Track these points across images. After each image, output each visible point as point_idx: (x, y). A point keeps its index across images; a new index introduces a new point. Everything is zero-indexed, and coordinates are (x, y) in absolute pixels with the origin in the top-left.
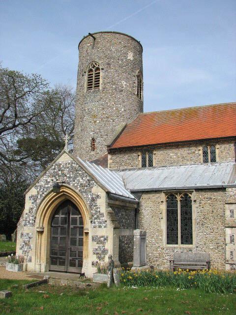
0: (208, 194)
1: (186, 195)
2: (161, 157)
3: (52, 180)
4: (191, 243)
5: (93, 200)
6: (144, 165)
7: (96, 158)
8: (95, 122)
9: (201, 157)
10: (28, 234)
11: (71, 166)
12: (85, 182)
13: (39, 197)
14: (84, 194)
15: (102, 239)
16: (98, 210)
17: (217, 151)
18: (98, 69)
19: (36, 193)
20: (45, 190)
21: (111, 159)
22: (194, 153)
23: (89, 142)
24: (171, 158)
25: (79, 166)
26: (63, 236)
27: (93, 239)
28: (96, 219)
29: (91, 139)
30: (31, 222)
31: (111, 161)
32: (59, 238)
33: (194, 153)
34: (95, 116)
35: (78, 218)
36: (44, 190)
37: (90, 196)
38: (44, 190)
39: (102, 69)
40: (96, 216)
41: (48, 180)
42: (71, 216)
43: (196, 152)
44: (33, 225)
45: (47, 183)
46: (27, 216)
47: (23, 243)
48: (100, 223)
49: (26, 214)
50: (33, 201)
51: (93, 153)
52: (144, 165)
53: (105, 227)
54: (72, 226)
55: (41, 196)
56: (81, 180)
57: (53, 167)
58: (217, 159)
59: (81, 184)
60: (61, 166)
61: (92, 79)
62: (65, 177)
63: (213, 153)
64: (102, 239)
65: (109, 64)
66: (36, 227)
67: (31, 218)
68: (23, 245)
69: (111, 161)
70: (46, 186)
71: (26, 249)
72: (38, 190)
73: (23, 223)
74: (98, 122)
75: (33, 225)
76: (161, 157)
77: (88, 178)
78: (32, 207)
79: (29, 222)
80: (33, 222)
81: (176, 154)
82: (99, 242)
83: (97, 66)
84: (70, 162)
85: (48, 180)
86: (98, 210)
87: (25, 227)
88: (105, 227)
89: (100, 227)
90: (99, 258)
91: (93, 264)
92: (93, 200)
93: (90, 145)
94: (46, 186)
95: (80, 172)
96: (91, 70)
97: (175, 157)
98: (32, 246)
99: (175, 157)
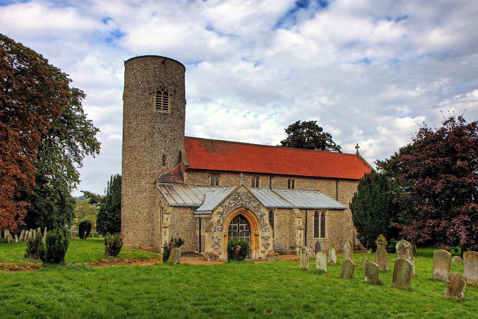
0: (283, 211)
1: (271, 211)
2: (225, 180)
3: (234, 202)
4: (324, 237)
5: (261, 216)
6: (212, 184)
7: (167, 173)
8: (166, 141)
9: (251, 183)
10: (217, 237)
11: (247, 194)
12: (256, 205)
13: (225, 213)
14: (256, 212)
15: (267, 238)
16: (265, 222)
17: (260, 181)
18: (166, 93)
19: (222, 211)
20: (229, 208)
21: (187, 176)
22: (247, 180)
23: (160, 157)
24: (232, 181)
25: (252, 195)
26: (234, 237)
27: (262, 238)
28: (263, 227)
29: (162, 155)
30: (219, 229)
31: (187, 178)
32: (245, 239)
33: (247, 180)
34: (165, 136)
35: (245, 226)
36: (228, 208)
37: (259, 214)
38: (228, 208)
39: (171, 95)
40: (263, 225)
41: (231, 202)
42: (240, 225)
43: (248, 180)
44: (221, 231)
45: (230, 204)
46: (216, 225)
47: (214, 243)
48: (266, 229)
49: (215, 224)
50: (220, 215)
51: (164, 167)
52: (212, 184)
53: (268, 231)
54: (241, 231)
55: (226, 212)
56: (254, 204)
57: (234, 194)
58: (260, 186)
59: (254, 206)
60: (240, 194)
61: (161, 101)
62: (243, 202)
63: (257, 182)
64: (267, 238)
65: (175, 92)
66: (223, 232)
67: (219, 227)
68: (214, 245)
69: (187, 178)
70: (230, 206)
71: (216, 247)
72: (224, 208)
73: (213, 230)
74: (168, 141)
75: (221, 231)
76: (225, 180)
77: (258, 203)
78: (219, 219)
79: (218, 229)
80: (221, 229)
81: (235, 179)
82: (266, 239)
83: (166, 90)
84: (246, 192)
85: (231, 202)
86: (265, 222)
87: (215, 233)
88: (268, 231)
89: (266, 231)
90: (266, 248)
91: (262, 252)
92: (261, 216)
93: (161, 160)
94: (230, 206)
95: (253, 199)
96: (159, 92)
97: (234, 181)
98: (221, 244)
99: (234, 181)
